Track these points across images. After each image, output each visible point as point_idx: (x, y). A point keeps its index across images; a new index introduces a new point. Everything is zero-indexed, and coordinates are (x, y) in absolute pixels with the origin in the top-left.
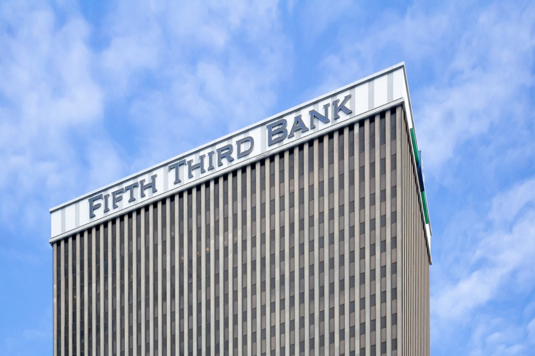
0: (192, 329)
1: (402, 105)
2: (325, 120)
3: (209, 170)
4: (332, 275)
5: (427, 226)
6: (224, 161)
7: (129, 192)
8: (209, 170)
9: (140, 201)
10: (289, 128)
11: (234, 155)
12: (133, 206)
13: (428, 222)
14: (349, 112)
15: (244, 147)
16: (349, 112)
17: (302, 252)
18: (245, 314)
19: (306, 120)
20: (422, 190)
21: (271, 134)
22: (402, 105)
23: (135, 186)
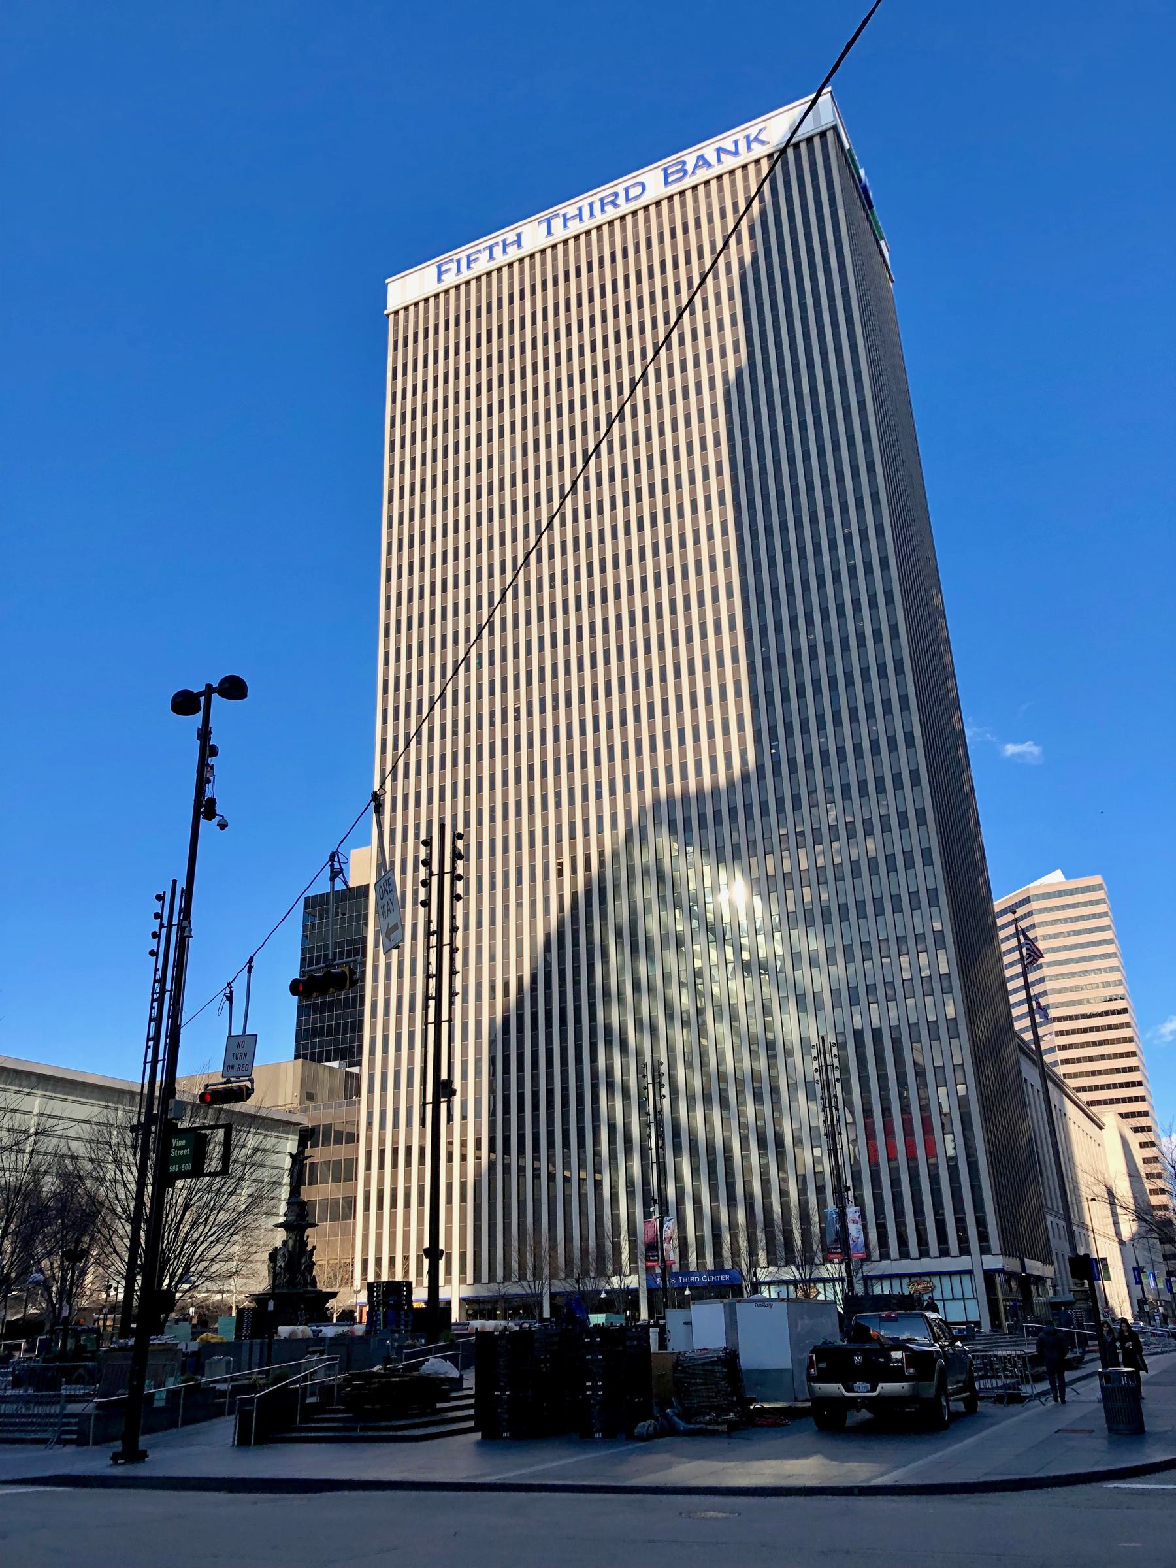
0: (844, 747)
1: (835, 128)
2: (736, 153)
3: (589, 219)
4: (433, 547)
5: (882, 243)
6: (609, 208)
7: (488, 252)
8: (589, 219)
9: (501, 259)
10: (689, 167)
11: (621, 200)
12: (493, 265)
13: (882, 239)
14: (763, 143)
15: (633, 192)
16: (763, 143)
17: (467, 574)
18: (396, 717)
19: (711, 156)
20: (871, 207)
21: (666, 176)
22: (835, 128)
23: (497, 244)
